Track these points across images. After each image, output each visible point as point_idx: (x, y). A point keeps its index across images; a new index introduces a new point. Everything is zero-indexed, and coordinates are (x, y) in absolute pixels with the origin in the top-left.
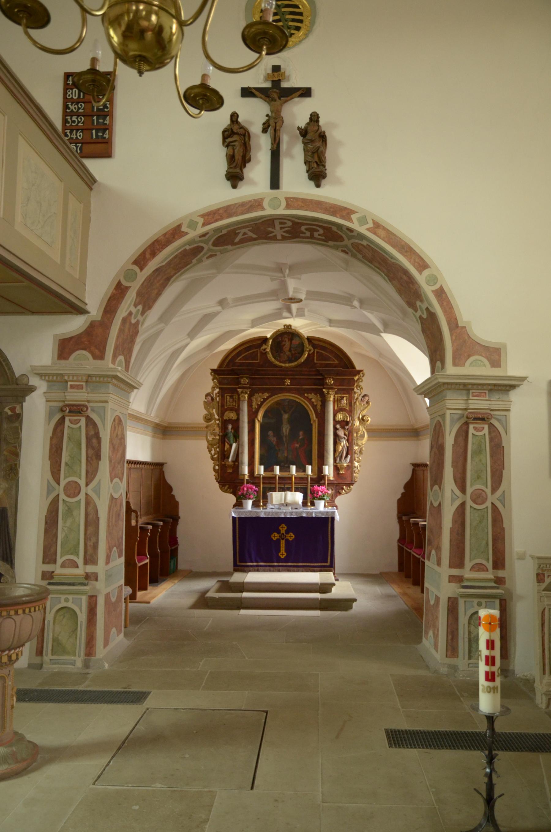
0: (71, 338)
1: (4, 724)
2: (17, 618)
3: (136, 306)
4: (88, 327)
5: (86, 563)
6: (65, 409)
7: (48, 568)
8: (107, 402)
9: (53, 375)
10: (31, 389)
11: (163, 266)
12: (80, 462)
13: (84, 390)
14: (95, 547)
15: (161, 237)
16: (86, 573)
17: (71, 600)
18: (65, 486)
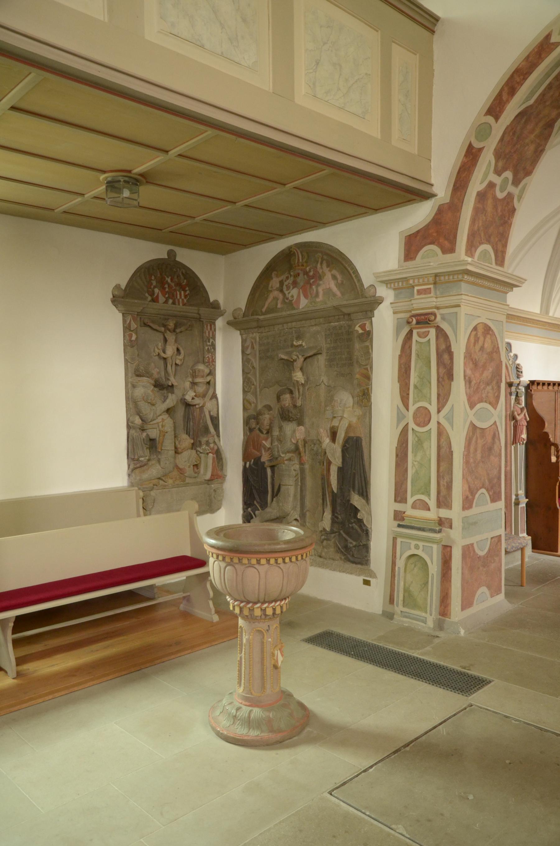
0: (418, 232)
1: (264, 684)
2: (263, 569)
3: (498, 173)
4: (436, 214)
5: (440, 505)
6: (410, 320)
7: (399, 507)
8: (459, 306)
9: (398, 280)
10: (378, 301)
11: (531, 106)
12: (430, 383)
13: (432, 295)
14: (449, 487)
15: (523, 63)
16: (439, 517)
17: (421, 548)
18: (414, 413)
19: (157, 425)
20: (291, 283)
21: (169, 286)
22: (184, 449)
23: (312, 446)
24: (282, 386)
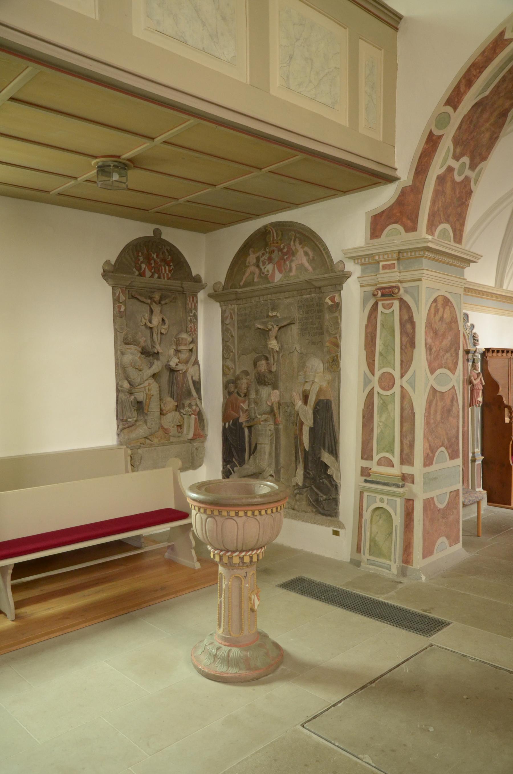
0: (383, 212)
2: (241, 520)
3: (456, 158)
4: (399, 196)
5: (403, 462)
6: (376, 293)
7: (366, 464)
8: (420, 280)
9: (364, 256)
10: (346, 276)
11: (487, 97)
12: (394, 350)
13: (396, 269)
14: (412, 446)
15: (479, 58)
16: (402, 473)
17: (386, 501)
18: (379, 378)
19: (143, 389)
20: (266, 259)
21: (155, 262)
22: (169, 411)
23: (286, 408)
24: (259, 353)
